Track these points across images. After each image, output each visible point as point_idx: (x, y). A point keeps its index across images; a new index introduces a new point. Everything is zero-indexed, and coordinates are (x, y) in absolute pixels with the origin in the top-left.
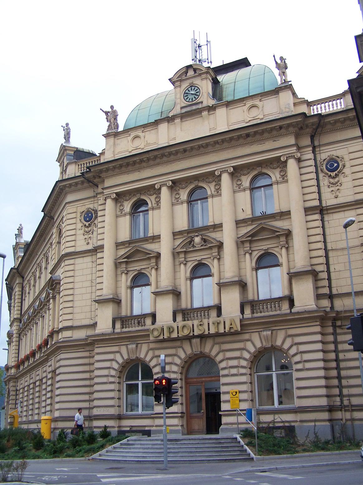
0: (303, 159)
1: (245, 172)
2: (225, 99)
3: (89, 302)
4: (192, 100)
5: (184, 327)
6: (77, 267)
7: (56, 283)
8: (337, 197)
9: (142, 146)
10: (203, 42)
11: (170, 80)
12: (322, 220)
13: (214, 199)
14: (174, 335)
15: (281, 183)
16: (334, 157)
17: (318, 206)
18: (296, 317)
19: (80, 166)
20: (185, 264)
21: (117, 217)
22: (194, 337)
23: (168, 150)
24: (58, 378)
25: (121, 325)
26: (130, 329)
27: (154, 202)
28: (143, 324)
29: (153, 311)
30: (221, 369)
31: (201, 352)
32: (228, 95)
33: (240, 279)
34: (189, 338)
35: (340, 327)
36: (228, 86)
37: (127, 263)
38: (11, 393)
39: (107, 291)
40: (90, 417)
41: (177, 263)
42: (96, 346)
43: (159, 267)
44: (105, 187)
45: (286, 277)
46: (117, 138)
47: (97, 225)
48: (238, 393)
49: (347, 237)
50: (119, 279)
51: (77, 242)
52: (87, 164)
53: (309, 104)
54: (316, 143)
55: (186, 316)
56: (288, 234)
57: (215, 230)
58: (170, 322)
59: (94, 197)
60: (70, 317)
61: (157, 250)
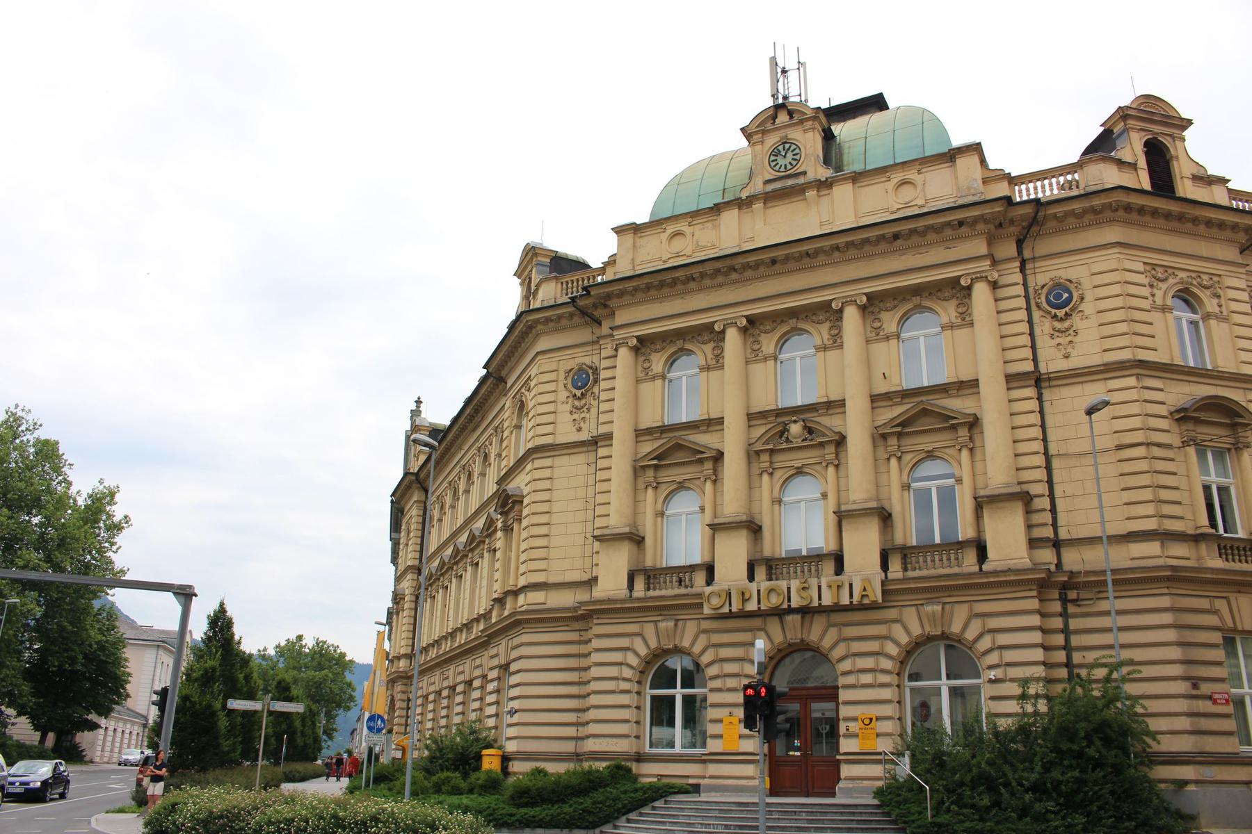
0: (1001, 283)
1: (888, 305)
2: (848, 170)
3: (579, 540)
4: (786, 168)
5: (771, 591)
6: (557, 473)
7: (514, 502)
8: (1067, 357)
9: (687, 252)
10: (791, 64)
11: (743, 130)
12: (1040, 398)
13: (827, 353)
14: (752, 606)
15: (959, 327)
16: (1061, 281)
17: (1032, 372)
18: (992, 580)
19: (564, 286)
20: (771, 474)
21: (638, 381)
22: (790, 611)
23: (741, 260)
24: (514, 680)
25: (645, 584)
26: (663, 592)
27: (710, 356)
28: (687, 583)
29: (707, 558)
30: (841, 675)
31: (802, 640)
32: (853, 160)
33: (879, 506)
34: (779, 613)
35: (1074, 601)
36: (852, 143)
37: (656, 467)
38: (398, 704)
39: (616, 520)
40: (578, 755)
41: (756, 471)
42: (596, 621)
43: (720, 477)
44: (616, 324)
45: (832, 519)
46: (639, 235)
47: (597, 394)
48: (874, 719)
49: (1092, 432)
50: (641, 497)
51: (558, 426)
52: (583, 282)
53: (1013, 181)
54: (1027, 254)
55: (774, 571)
56: (974, 423)
57: (830, 412)
58: (743, 582)
59: (593, 343)
60: (541, 565)
61: (716, 446)
